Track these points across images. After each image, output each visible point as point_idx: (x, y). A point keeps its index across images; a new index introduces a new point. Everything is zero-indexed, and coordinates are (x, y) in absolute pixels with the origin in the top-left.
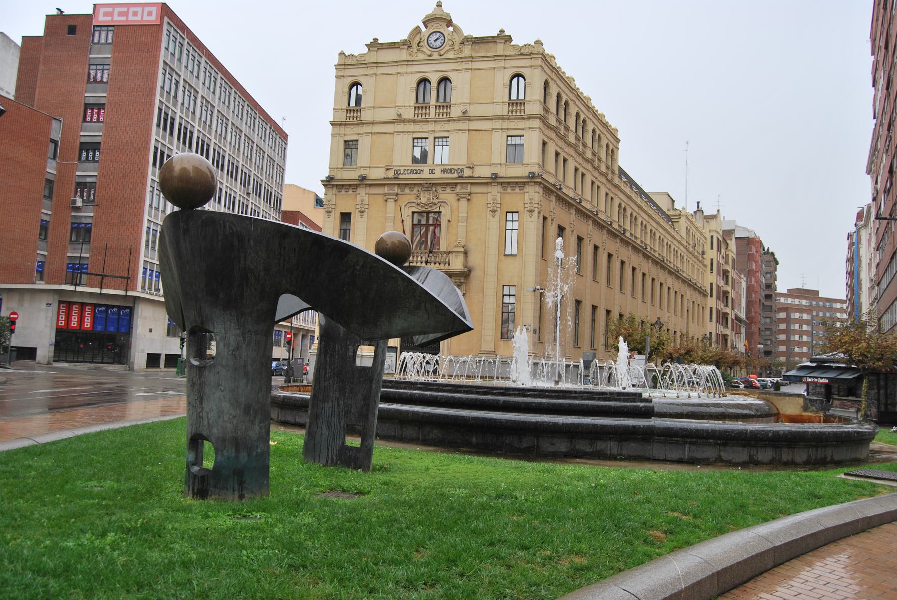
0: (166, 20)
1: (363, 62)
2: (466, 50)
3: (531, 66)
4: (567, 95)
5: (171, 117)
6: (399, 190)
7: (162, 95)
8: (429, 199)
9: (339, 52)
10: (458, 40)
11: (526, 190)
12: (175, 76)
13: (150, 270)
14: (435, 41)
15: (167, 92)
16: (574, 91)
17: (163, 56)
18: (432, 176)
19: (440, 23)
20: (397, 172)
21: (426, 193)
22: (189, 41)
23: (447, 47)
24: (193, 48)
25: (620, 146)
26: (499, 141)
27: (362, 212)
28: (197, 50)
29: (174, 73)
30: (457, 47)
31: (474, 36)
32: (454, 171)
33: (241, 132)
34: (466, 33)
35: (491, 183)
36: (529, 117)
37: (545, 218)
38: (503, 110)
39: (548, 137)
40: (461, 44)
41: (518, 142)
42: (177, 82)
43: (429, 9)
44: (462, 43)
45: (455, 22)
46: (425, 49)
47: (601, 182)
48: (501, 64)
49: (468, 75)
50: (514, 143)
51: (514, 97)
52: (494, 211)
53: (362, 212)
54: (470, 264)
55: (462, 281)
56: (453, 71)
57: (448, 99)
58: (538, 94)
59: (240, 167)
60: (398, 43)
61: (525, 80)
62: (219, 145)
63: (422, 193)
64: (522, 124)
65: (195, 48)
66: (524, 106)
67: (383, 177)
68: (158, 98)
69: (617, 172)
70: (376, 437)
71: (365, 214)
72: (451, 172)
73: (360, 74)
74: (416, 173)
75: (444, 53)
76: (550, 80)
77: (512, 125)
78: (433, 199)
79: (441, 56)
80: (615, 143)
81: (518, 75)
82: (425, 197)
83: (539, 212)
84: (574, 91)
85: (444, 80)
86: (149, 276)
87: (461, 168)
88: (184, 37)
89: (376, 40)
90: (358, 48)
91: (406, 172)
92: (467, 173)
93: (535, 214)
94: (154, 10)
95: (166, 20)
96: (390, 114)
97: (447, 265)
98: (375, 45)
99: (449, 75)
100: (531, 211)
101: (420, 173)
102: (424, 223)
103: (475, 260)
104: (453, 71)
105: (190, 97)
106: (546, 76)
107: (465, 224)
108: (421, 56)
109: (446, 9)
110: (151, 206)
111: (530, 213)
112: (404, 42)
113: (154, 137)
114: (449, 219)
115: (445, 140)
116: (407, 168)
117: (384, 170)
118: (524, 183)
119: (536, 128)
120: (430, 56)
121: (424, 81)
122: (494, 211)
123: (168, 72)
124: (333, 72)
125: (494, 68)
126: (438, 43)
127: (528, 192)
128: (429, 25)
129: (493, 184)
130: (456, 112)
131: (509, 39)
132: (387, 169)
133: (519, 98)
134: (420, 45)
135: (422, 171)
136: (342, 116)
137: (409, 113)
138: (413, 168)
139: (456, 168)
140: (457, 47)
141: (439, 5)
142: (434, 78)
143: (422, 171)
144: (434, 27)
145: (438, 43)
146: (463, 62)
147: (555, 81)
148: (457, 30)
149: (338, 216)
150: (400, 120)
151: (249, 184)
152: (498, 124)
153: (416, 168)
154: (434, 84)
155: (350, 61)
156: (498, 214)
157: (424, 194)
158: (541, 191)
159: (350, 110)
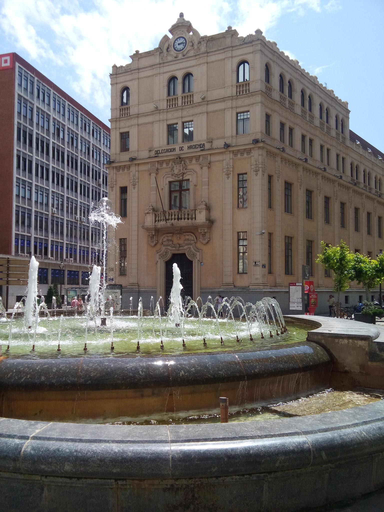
0: (17, 64)
1: (129, 70)
2: (203, 48)
3: (253, 52)
4: (291, 75)
5: (29, 134)
6: (159, 166)
7: (19, 117)
8: (180, 170)
9: (113, 65)
11: (252, 154)
12: (29, 104)
13: (87, 251)
14: (179, 44)
15: (23, 116)
16: (298, 72)
17: (17, 91)
18: (182, 152)
19: (182, 29)
21: (178, 166)
22: (38, 79)
23: (188, 47)
24: (42, 84)
25: (351, 115)
26: (230, 117)
27: (134, 185)
28: (46, 85)
29: (28, 102)
30: (196, 47)
31: (208, 35)
32: (197, 146)
33: (90, 142)
34: (202, 34)
35: (225, 152)
37: (270, 177)
39: (272, 110)
40: (198, 43)
41: (245, 117)
42: (32, 110)
43: (174, 21)
44: (199, 43)
45: (194, 26)
46: (173, 52)
47: (331, 145)
49: (204, 67)
50: (242, 117)
51: (241, 80)
52: (228, 174)
54: (212, 218)
55: (206, 231)
56: (193, 66)
57: (192, 89)
58: (260, 74)
59: (91, 166)
60: (152, 51)
61: (249, 65)
62: (72, 152)
63: (175, 166)
64: (247, 101)
65: (44, 84)
66: (249, 86)
67: (147, 157)
68: (16, 120)
69: (348, 137)
70: (85, 330)
71: (137, 186)
72: (195, 148)
73: (335, 124)
74: (171, 151)
75: (186, 54)
76: (271, 63)
77: (240, 102)
78: (183, 170)
79: (184, 56)
80: (345, 113)
81: (243, 62)
82: (177, 169)
83: (263, 172)
84: (298, 72)
85: (188, 76)
86: (27, 244)
87: (202, 143)
88: (33, 76)
89: (137, 52)
90: (124, 61)
91: (163, 151)
93: (260, 173)
94: (8, 58)
95: (17, 64)
97: (194, 220)
99: (191, 70)
100: (257, 171)
101: (173, 151)
102: (178, 189)
103: (215, 214)
104: (193, 66)
105: (44, 119)
106: (265, 60)
107: (207, 187)
108: (170, 58)
110: (18, 196)
111: (256, 173)
112: (156, 50)
113: (16, 147)
114: (195, 184)
115: (190, 123)
116: (164, 149)
117: (148, 151)
118: (250, 149)
119: (258, 103)
120: (176, 57)
121: (173, 79)
122: (228, 174)
123: (22, 102)
125: (224, 59)
126: (181, 46)
127: (253, 156)
128: (175, 33)
129: (226, 153)
130: (197, 99)
132: (150, 151)
133: (240, 81)
134: (169, 50)
135: (174, 149)
138: (168, 148)
139: (199, 143)
141: (182, 15)
142: (180, 75)
143: (174, 149)
144: (179, 33)
145: (181, 46)
146: (200, 58)
147: (277, 63)
148: (195, 32)
149: (118, 190)
151: (99, 178)
152: (229, 104)
153: (170, 148)
154: (180, 80)
155: (120, 71)
156: (231, 176)
157: (176, 166)
158: (265, 154)
159: (123, 109)
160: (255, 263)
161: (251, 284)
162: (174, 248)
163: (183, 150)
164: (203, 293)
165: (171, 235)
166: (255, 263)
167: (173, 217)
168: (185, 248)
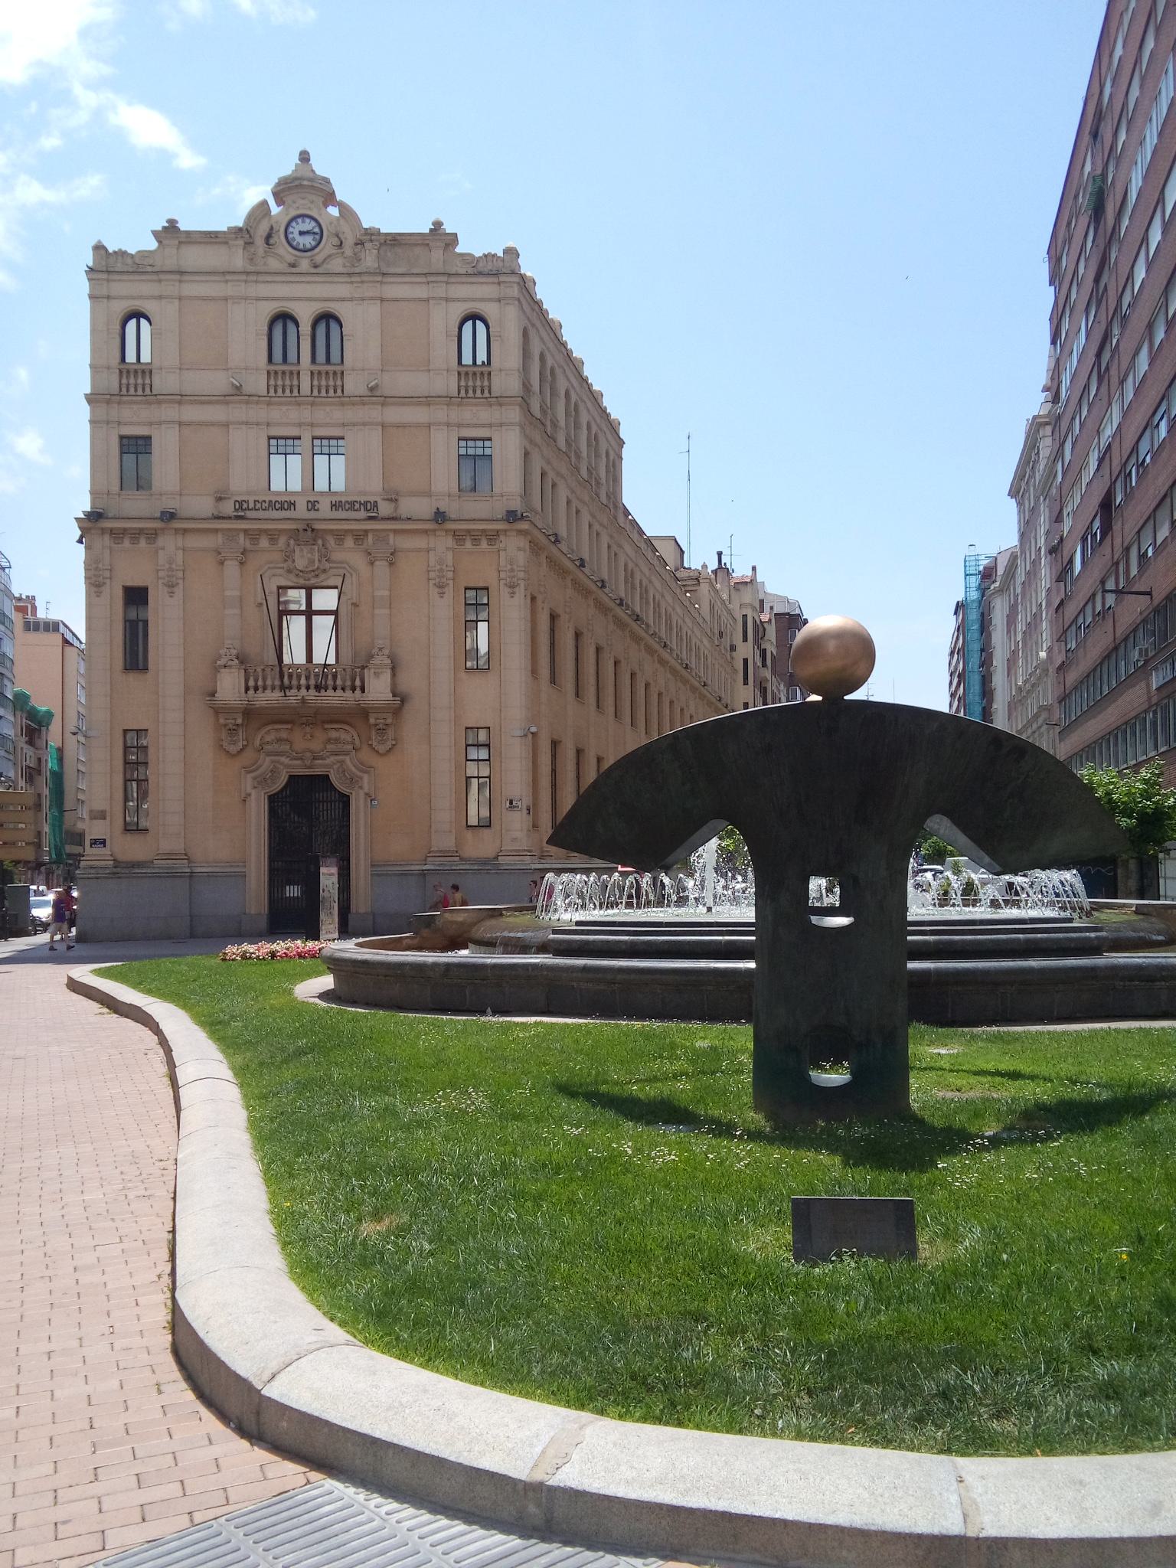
10: (349, 240)
20: (240, 505)
36: (500, 401)
37: (533, 599)
38: (447, 384)
43: (288, 166)
44: (360, 243)
48: (440, 291)
49: (374, 310)
53: (171, 586)
82: (302, 556)
85: (326, 319)
91: (258, 505)
92: (385, 509)
96: (217, 382)
98: (170, 232)
103: (410, 681)
108: (274, 264)
109: (320, 166)
112: (237, 232)
124: (84, 286)
130: (354, 384)
131: (453, 239)
136: (112, 382)
137: (257, 383)
139: (363, 499)
140: (348, 250)
142: (306, 314)
150: (236, 394)
152: (440, 413)
154: (305, 328)
160: (511, 803)
161: (430, 853)
162: (298, 762)
163: (318, 510)
164: (379, 875)
165: (289, 726)
166: (511, 803)
167: (303, 681)
168: (328, 761)
